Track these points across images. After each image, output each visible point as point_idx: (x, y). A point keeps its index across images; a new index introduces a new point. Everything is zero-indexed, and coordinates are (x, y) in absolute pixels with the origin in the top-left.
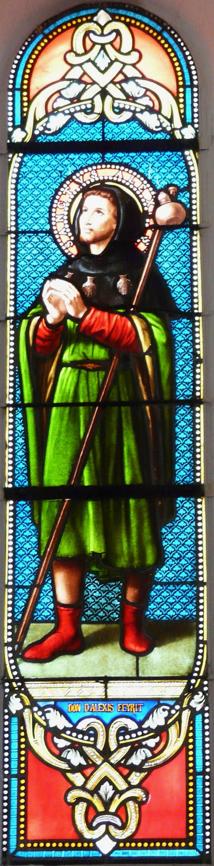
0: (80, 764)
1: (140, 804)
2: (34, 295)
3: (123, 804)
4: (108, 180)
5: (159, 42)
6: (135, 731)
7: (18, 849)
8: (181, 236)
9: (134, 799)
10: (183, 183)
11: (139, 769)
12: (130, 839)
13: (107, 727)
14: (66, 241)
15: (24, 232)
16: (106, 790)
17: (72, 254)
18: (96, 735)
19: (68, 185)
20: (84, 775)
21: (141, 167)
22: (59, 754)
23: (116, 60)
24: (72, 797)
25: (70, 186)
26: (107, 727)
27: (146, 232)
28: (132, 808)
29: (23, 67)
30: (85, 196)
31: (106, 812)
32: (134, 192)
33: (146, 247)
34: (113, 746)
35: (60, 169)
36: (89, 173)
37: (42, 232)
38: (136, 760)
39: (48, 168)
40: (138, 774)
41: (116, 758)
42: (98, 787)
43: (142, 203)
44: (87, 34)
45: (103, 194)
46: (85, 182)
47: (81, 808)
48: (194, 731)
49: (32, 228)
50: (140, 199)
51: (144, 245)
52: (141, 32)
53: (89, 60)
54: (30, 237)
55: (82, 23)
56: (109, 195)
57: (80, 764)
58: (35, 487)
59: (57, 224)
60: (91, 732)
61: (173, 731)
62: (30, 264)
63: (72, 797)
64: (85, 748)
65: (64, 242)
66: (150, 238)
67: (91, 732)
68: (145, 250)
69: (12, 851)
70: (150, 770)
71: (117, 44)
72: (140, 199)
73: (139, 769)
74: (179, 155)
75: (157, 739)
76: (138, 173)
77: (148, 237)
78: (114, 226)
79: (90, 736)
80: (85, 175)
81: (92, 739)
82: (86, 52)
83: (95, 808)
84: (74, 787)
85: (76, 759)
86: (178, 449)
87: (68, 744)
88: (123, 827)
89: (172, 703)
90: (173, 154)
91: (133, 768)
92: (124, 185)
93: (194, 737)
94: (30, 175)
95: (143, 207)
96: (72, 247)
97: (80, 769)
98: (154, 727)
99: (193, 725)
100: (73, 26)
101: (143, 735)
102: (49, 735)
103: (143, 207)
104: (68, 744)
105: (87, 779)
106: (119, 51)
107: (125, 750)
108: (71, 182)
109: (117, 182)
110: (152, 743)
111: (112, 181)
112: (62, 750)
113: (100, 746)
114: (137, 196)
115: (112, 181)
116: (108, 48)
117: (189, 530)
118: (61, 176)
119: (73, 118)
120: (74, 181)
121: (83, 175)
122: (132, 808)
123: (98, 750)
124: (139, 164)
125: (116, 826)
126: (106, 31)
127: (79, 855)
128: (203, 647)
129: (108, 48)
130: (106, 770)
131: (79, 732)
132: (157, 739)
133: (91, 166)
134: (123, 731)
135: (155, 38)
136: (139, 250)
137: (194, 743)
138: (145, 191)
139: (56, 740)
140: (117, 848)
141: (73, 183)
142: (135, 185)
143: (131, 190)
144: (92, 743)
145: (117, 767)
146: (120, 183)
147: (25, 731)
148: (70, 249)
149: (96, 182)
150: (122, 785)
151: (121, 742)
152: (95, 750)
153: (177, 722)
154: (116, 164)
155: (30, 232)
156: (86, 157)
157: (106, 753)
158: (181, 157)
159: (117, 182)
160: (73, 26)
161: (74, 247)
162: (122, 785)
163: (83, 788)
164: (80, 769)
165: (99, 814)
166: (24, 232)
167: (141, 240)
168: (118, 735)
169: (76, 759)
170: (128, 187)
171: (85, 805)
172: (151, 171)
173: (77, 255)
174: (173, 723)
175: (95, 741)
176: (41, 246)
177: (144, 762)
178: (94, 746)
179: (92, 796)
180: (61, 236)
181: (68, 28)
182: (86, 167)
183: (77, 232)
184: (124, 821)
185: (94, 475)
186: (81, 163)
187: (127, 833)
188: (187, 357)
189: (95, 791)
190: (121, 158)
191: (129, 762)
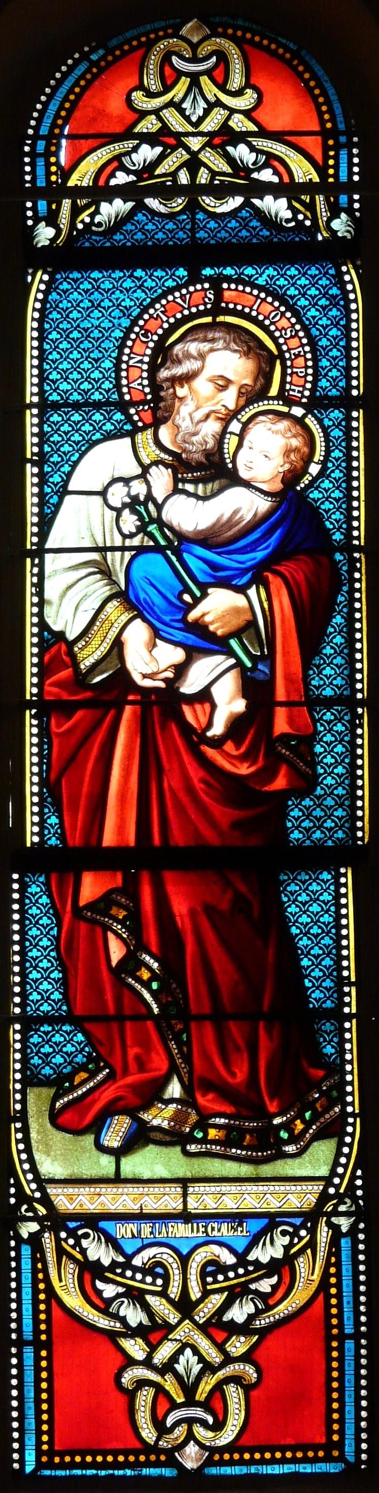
0: (141, 1323)
1: (248, 1389)
2: (77, 451)
3: (218, 1388)
5: (295, 69)
6: (234, 1268)
7: (39, 1465)
8: (331, 333)
9: (236, 1379)
11: (244, 1329)
12: (230, 1448)
13: (184, 1260)
15: (56, 406)
16: (188, 1363)
18: (166, 1278)
20: (148, 1343)
22: (105, 1307)
23: (219, 103)
24: (128, 1378)
26: (184, 1260)
28: (234, 1396)
29: (25, 1321)
31: (190, 1402)
34: (195, 1293)
38: (239, 1313)
40: (242, 1339)
41: (204, 1312)
42: (174, 1358)
44: (166, 59)
47: (145, 1398)
48: (338, 1265)
52: (265, 55)
53: (171, 104)
55: (159, 39)
57: (141, 1323)
58: (74, 849)
60: (153, 1269)
61: (302, 1264)
62: (69, 439)
63: (128, 1378)
64: (148, 1298)
67: (159, 1270)
69: (29, 1469)
70: (263, 1333)
71: (219, 74)
73: (244, 1329)
75: (274, 1280)
79: (155, 1276)
81: (159, 1282)
82: (167, 89)
83: (167, 1394)
84: (130, 1362)
85: (134, 1316)
86: (322, 782)
87: (121, 1290)
88: (219, 1426)
89: (298, 1221)
91: (234, 1329)
93: (338, 1275)
97: (140, 1332)
98: (265, 1259)
99: (338, 1255)
100: (141, 45)
101: (247, 1273)
102: (87, 1277)
104: (121, 1290)
105: (153, 1348)
106: (222, 87)
107: (217, 1300)
110: (265, 1286)
112: (110, 1301)
113: (174, 1291)
116: (205, 80)
117: (334, 312)
119: (140, 207)
121: (191, 293)
122: (234, 1396)
123: (170, 1301)
125: (204, 1423)
126: (202, 51)
129: (205, 80)
130: (185, 1331)
131: (135, 1269)
132: (274, 1280)
134: (213, 1268)
135: (288, 63)
137: (339, 1285)
139: (100, 1285)
140: (209, 1462)
144: (160, 1289)
145: (205, 1329)
147: (45, 1270)
150: (215, 1357)
151: (209, 1287)
152: (164, 1301)
153: (309, 1251)
157: (185, 1306)
160: (141, 45)
162: (215, 1357)
163: (148, 1363)
164: (140, 1332)
165: (174, 1406)
166: (56, 406)
168: (203, 1274)
169: (134, 1316)
171: (152, 1391)
174: (302, 1251)
175: (166, 1285)
177: (251, 1318)
178: (163, 1294)
179: (163, 1376)
181: (133, 49)
184: (221, 1418)
185: (197, 766)
187: (227, 1436)
189: (168, 1367)
191: (227, 1317)
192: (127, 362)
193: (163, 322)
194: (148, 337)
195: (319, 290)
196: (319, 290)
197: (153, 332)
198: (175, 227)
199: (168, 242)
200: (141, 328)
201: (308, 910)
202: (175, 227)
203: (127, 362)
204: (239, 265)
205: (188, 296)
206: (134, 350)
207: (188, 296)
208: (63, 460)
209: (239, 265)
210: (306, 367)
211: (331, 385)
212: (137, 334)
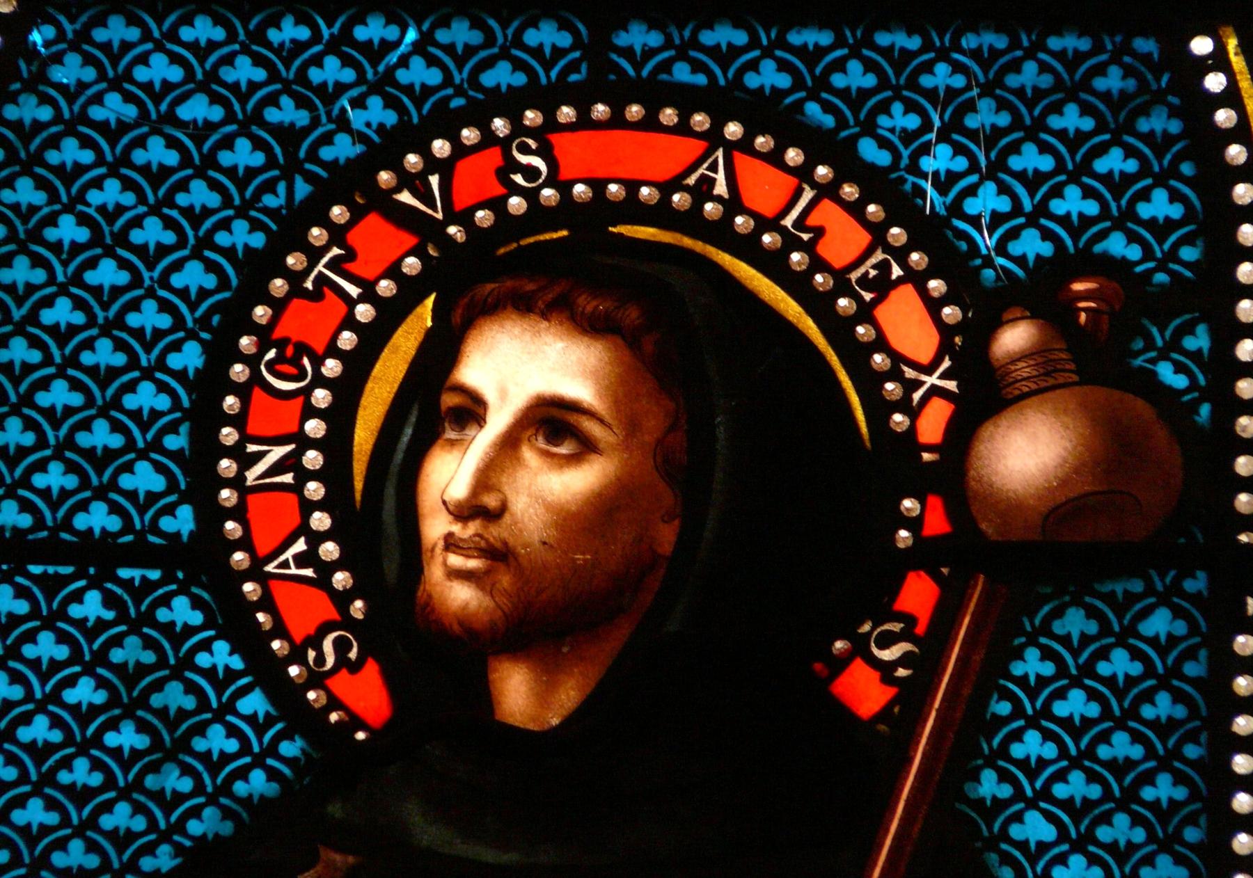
4: (633, 210)
10: (1172, 255)
14: (311, 629)
17: (359, 724)
19: (338, 234)
21: (869, 128)
25: (353, 237)
27: (894, 589)
30: (457, 317)
32: (818, 305)
33: (890, 692)
35: (287, 113)
36: (493, 157)
37: (140, 554)
39: (197, 109)
43: (869, 382)
45: (587, 304)
46: (464, 218)
49: (67, 524)
50: (856, 355)
51: (874, 675)
54: (51, 585)
56: (632, 315)
59: (252, 499)
65: (300, 628)
66: (920, 629)
68: (884, 714)
72: (856, 355)
74: (1146, 58)
76: (849, 167)
77: (909, 620)
78: (666, 536)
80: (463, 166)
90: (1098, 48)
92: (748, 248)
94: (71, 152)
95: (878, 409)
96: (355, 668)
103: (878, 409)
108: (357, 215)
109: (691, 222)
111: (661, 215)
114: (837, 329)
115: (661, 215)
118: (291, 169)
120: (384, 204)
121: (445, 168)
124: (856, 104)
127: (163, 728)
128: (1220, 49)
133: (511, 104)
136: (842, 713)
138: (895, 295)
141: (373, 221)
142: (824, 249)
143: (797, 285)
146: (721, 233)
148: (342, 684)
149: (538, 216)
154: (687, 100)
155: (51, 551)
156: (476, 37)
158: (1157, 72)
159: (691, 222)
161: (371, 670)
167: (860, 649)
170: (773, 265)
172: (940, 159)
173: (390, 725)
176: (130, 652)
180: (281, 593)
182: (480, 117)
183: (391, 567)
186: (434, 77)
188: (1163, 789)
190: (725, 56)
192: (237, 483)
193: (351, 303)
194: (301, 376)
195: (43, 347)
196: (43, 347)
197: (320, 348)
198: (79, 318)
199: (448, 99)
200: (264, 336)
201: (113, 485)
202: (79, 318)
203: (316, 539)
204: (505, 13)
205: (434, 180)
206: (253, 428)
207: (434, 180)
208: (42, 443)
209: (505, 13)
210: (804, 174)
211: (1151, 837)
212: (252, 361)
